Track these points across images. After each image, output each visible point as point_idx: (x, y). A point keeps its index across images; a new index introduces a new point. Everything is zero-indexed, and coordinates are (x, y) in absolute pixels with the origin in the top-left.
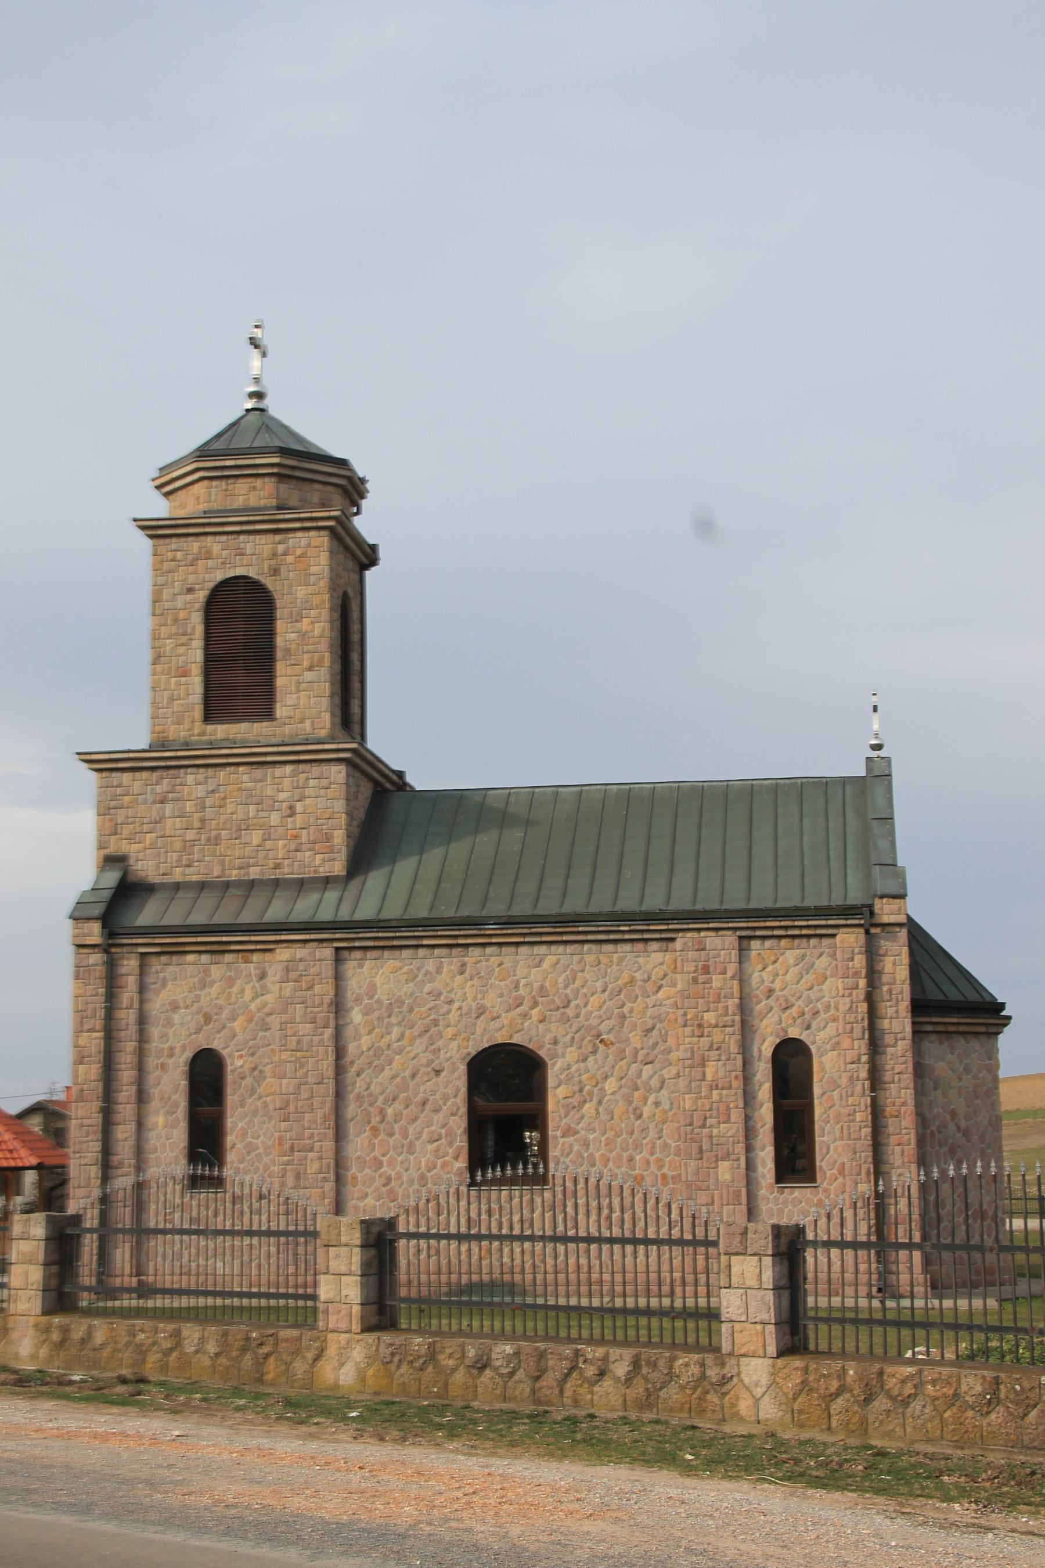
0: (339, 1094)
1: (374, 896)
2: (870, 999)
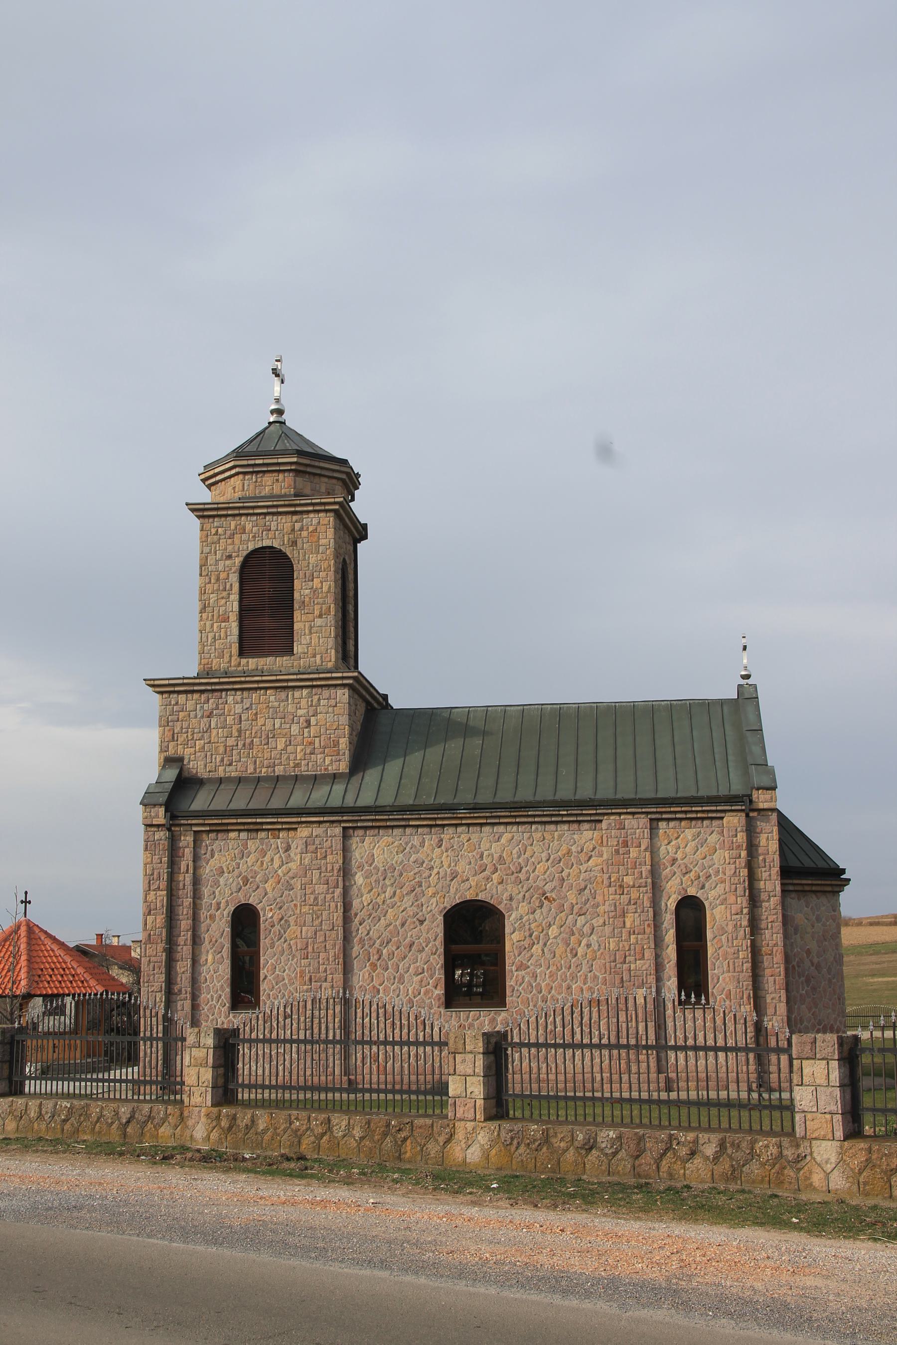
0: (347, 938)
1: (370, 788)
2: (750, 866)
